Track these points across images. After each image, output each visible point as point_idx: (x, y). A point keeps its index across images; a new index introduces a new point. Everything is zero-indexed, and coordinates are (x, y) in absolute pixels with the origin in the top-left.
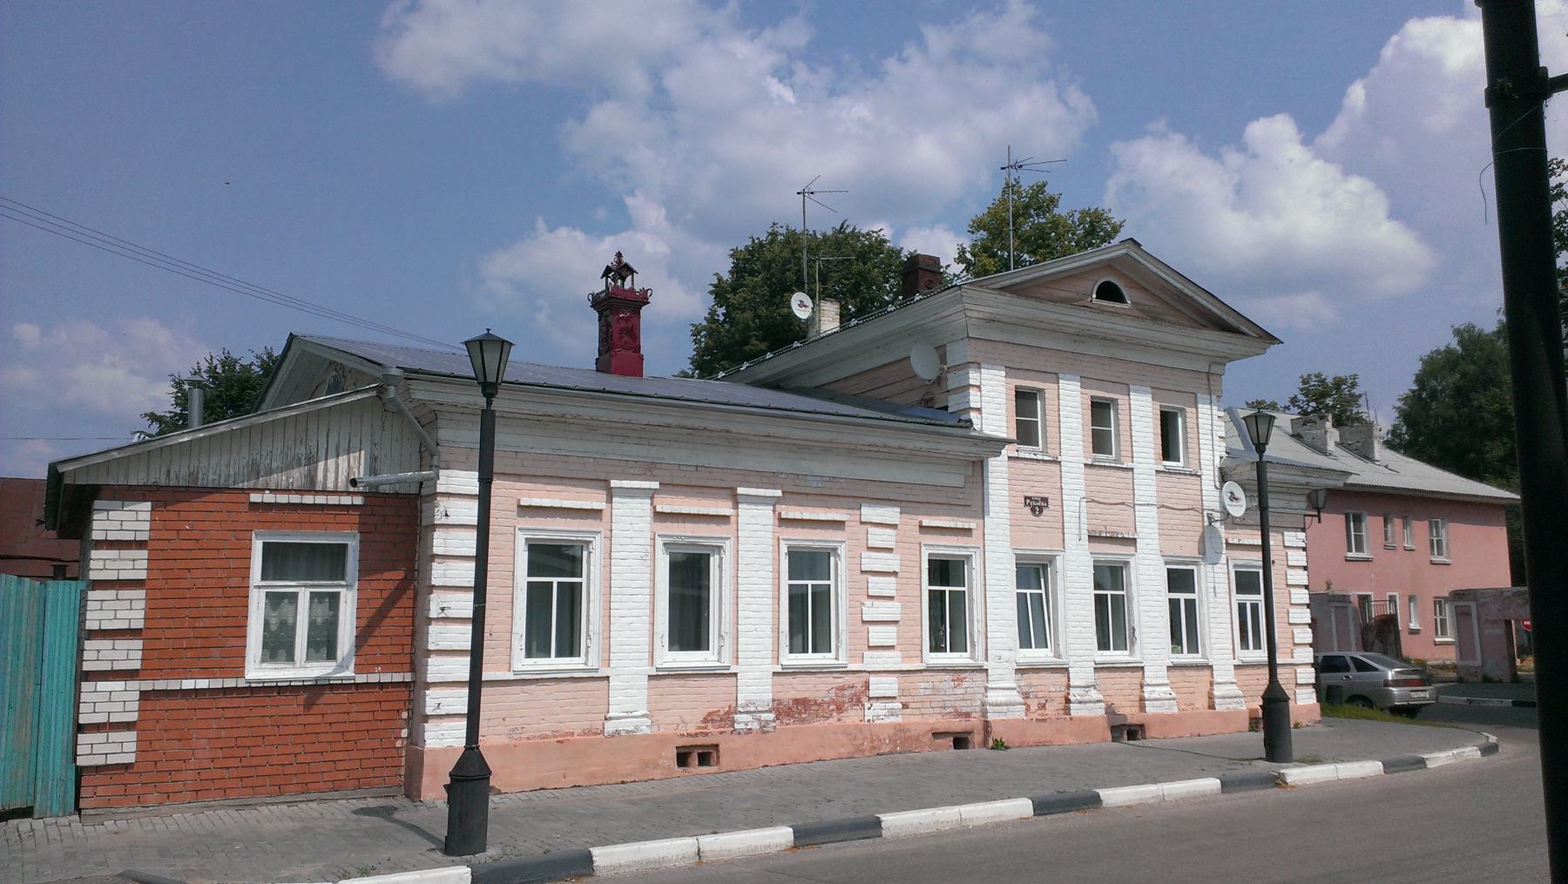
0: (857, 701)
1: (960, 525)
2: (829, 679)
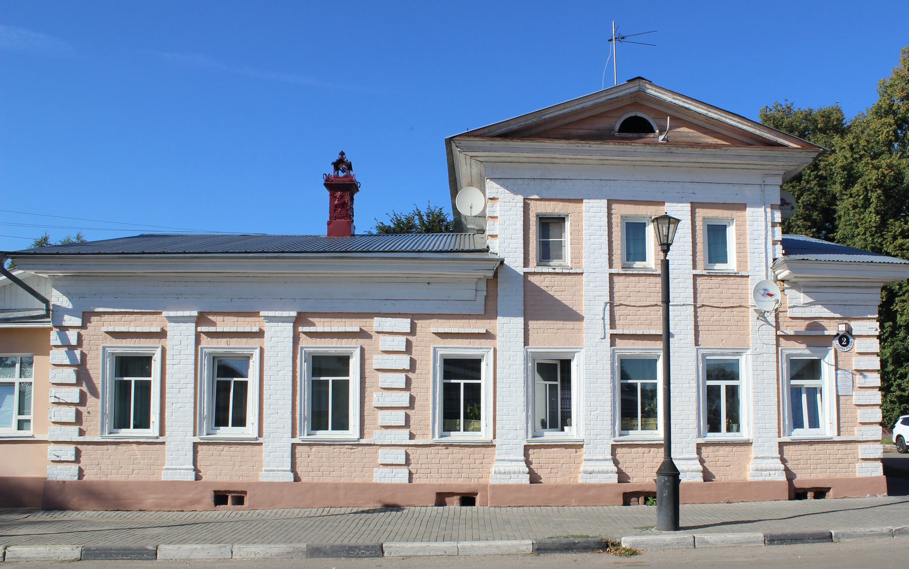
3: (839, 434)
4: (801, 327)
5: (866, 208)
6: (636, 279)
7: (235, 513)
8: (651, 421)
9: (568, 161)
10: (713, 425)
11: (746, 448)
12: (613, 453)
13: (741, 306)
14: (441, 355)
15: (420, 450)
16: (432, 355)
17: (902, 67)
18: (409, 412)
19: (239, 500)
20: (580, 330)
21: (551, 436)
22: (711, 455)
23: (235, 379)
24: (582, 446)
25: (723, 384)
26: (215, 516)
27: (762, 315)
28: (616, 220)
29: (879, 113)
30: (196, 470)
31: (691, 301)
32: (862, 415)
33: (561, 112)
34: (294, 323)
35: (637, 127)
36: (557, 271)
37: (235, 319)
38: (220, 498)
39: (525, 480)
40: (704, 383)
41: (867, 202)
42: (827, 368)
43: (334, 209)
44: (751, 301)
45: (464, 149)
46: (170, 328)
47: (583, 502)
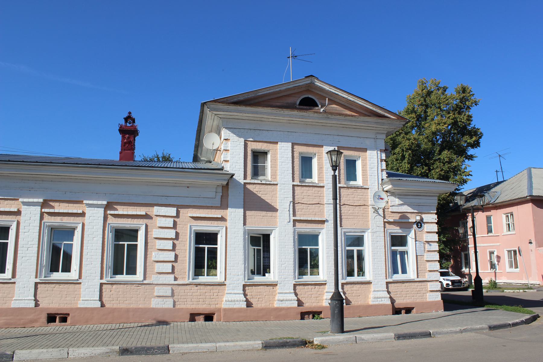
3: (418, 277)
4: (397, 217)
5: (402, 161)
6: (307, 188)
7: (62, 327)
8: (315, 270)
9: (270, 120)
11: (368, 285)
12: (295, 289)
14: (194, 230)
15: (180, 287)
16: (189, 230)
17: (419, 89)
18: (174, 264)
19: (64, 319)
20: (276, 217)
21: (258, 279)
22: (349, 289)
23: (65, 242)
24: (276, 285)
25: (355, 249)
26: (48, 330)
27: (376, 211)
28: (296, 155)
29: (408, 112)
30: (36, 300)
33: (268, 92)
34: (105, 208)
35: (308, 103)
36: (263, 182)
37: (67, 205)
38: (51, 318)
39: (244, 305)
40: (345, 248)
41: (403, 157)
42: (410, 240)
43: (123, 145)
44: (371, 201)
45: (212, 110)
46: (24, 209)
47: (278, 318)
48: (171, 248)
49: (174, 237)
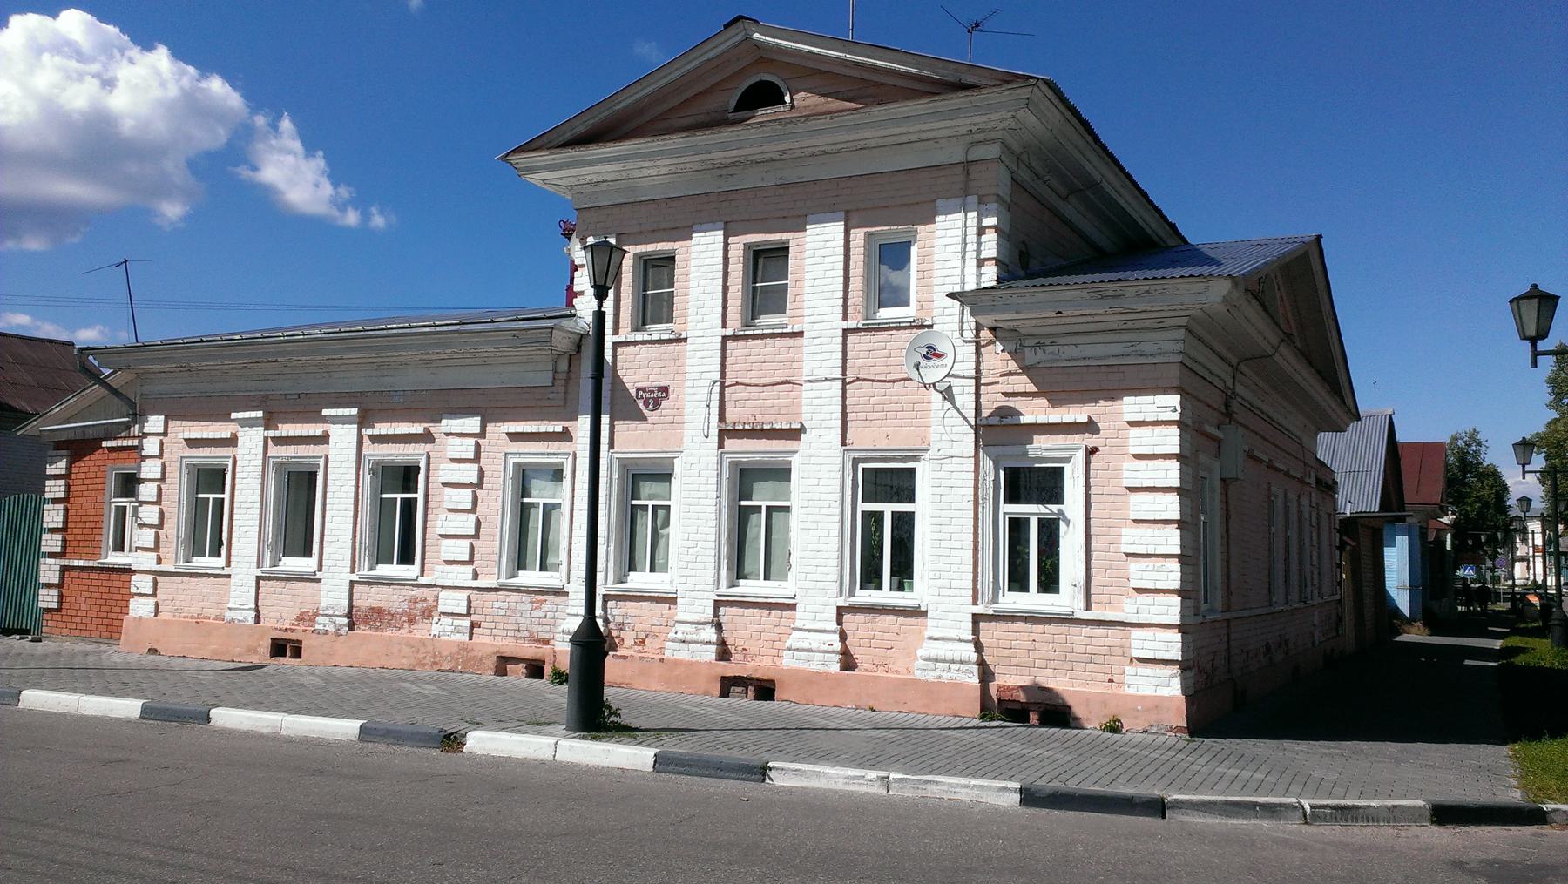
0: (428, 614)
1: (542, 429)
2: (404, 591)
3: (1088, 607)
10: (871, 577)
13: (787, 382)
15: (486, 596)
25: (888, 509)
31: (838, 373)
32: (1143, 575)
48: (469, 506)
49: (475, 481)
